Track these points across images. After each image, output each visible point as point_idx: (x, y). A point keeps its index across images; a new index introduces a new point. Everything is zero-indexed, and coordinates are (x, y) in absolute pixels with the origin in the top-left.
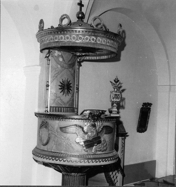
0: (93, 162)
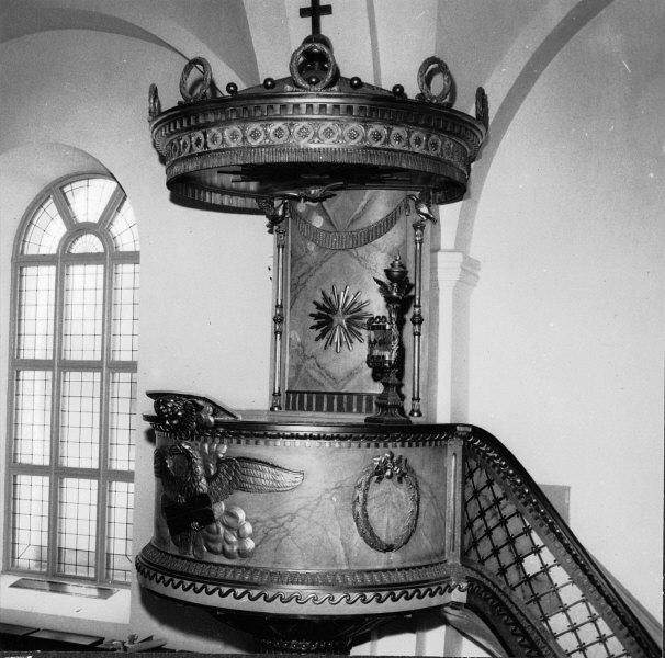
0: (353, 599)
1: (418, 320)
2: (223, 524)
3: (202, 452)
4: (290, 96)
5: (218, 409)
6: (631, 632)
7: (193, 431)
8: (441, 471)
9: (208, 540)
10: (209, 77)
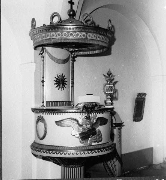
0: (89, 153)
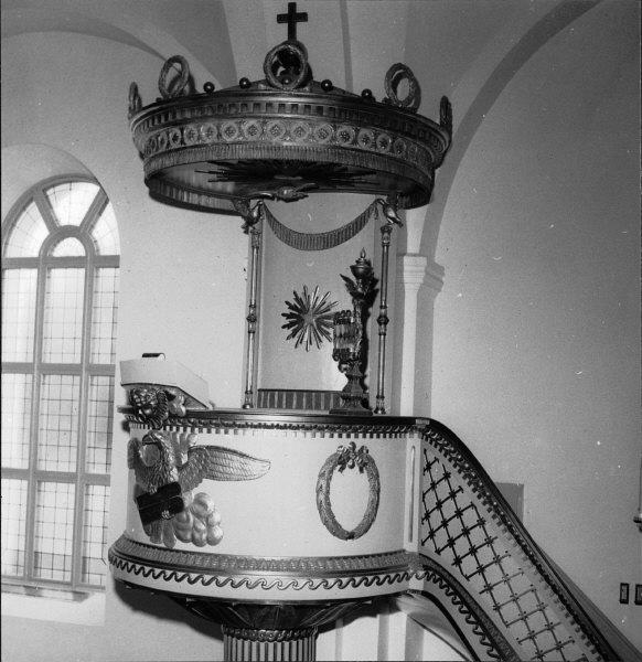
0: (315, 585)
1: (383, 320)
2: (193, 513)
3: (174, 442)
4: (264, 95)
5: (189, 399)
6: (576, 620)
7: (165, 421)
8: (399, 463)
9: (178, 528)
10: (187, 75)
